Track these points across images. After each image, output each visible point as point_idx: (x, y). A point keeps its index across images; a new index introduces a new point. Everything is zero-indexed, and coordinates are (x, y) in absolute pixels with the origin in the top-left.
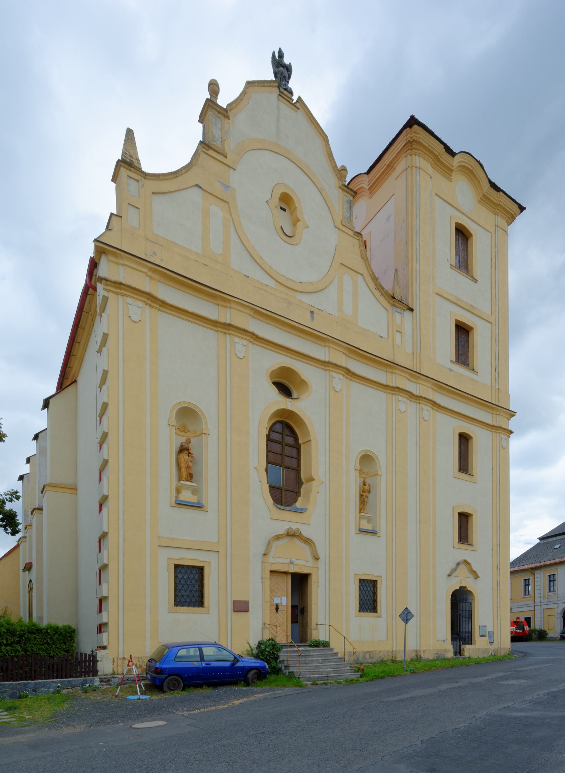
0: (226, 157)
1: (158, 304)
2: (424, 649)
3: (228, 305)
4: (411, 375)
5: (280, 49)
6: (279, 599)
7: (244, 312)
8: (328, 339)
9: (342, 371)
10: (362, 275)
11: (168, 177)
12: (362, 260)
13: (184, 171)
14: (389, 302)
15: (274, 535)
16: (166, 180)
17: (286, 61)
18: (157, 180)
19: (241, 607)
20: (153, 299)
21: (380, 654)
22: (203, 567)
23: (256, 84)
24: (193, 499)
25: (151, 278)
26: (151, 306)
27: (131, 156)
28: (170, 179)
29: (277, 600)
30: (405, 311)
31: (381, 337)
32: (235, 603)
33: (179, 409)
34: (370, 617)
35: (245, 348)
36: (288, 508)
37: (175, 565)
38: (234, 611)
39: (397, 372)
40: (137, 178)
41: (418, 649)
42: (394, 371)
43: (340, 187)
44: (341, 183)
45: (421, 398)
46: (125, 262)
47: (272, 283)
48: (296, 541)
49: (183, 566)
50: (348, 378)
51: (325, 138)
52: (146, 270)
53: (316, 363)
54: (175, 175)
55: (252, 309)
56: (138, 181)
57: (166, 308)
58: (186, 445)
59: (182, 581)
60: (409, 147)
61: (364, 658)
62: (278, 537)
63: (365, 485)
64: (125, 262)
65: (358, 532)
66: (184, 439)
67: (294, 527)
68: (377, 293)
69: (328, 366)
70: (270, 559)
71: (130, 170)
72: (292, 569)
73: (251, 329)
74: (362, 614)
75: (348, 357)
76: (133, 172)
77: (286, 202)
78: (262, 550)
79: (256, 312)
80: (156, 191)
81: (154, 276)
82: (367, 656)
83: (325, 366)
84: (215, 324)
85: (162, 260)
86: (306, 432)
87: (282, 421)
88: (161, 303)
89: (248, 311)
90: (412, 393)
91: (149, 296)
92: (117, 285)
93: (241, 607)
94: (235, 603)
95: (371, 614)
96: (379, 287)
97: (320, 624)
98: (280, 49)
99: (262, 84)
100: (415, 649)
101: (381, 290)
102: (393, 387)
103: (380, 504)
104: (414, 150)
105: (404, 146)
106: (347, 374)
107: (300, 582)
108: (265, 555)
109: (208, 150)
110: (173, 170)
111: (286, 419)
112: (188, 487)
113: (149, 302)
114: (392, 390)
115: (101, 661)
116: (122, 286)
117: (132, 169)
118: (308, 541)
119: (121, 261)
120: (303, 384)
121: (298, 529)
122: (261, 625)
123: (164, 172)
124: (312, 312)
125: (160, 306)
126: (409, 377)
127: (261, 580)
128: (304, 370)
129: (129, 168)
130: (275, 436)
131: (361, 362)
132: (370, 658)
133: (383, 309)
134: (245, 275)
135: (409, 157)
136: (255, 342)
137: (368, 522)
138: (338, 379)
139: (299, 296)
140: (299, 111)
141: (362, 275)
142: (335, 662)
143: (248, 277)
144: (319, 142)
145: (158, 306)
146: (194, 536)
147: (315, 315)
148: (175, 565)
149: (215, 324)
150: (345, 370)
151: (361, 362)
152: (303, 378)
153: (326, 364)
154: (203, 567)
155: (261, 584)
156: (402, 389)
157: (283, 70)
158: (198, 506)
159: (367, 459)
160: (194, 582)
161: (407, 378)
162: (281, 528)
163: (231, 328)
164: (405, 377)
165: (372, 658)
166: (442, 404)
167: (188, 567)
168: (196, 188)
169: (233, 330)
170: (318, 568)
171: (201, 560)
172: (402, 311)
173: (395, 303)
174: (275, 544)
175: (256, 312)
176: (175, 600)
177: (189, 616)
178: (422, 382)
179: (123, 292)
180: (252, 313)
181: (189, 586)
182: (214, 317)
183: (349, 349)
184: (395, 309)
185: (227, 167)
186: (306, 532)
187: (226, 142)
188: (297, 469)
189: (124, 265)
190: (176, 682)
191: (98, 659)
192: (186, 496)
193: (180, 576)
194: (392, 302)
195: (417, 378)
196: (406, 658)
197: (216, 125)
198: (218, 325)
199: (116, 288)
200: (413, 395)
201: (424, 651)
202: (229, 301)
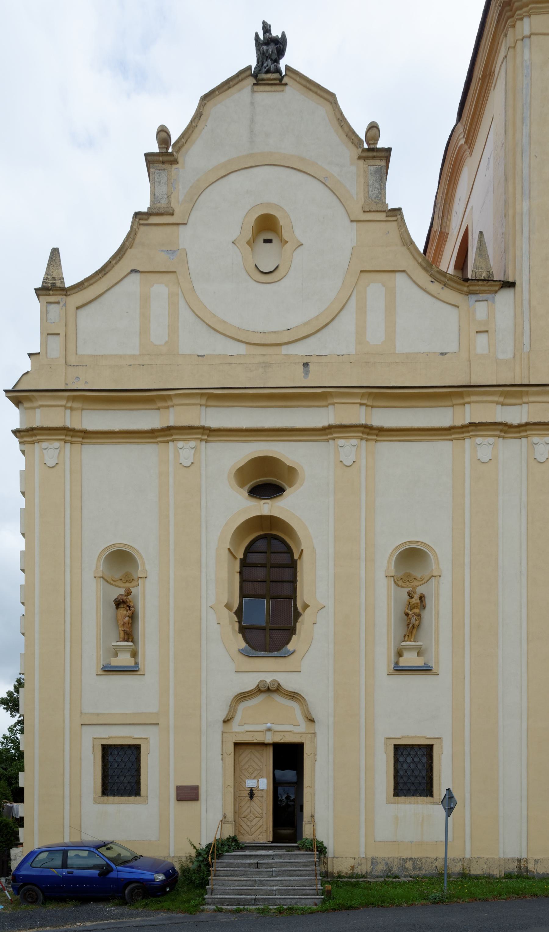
0: (172, 214)
1: (79, 437)
2: (537, 857)
3: (169, 403)
4: (506, 395)
5: (264, 23)
6: (255, 781)
7: (193, 404)
8: (329, 392)
9: (358, 432)
10: (404, 271)
11: (94, 280)
12: (404, 249)
13: (113, 262)
14: (461, 292)
15: (234, 695)
16: (92, 284)
17: (276, 33)
18: (81, 290)
19: (188, 794)
20: (71, 433)
21: (436, 864)
22: (140, 745)
23: (217, 92)
24: (419, 662)
25: (71, 409)
26: (72, 443)
27: (54, 279)
28: (97, 281)
29: (250, 783)
30: (496, 292)
31: (442, 354)
32: (179, 789)
33: (106, 557)
34: (418, 803)
35: (193, 450)
36: (276, 654)
37: (395, 745)
38: (178, 800)
39: (473, 398)
40: (57, 301)
41: (524, 856)
42: (467, 400)
43: (359, 158)
44: (360, 150)
45: (528, 427)
46: (40, 403)
47: (242, 349)
48: (278, 698)
49: (405, 746)
50: (372, 440)
51: (331, 99)
52: (63, 403)
53: (111, 438)
54: (103, 272)
55: (202, 395)
56: (58, 303)
57: (90, 438)
58: (124, 598)
59: (418, 765)
60: (509, 14)
61: (404, 869)
62: (243, 697)
63: (411, 597)
64: (40, 403)
65: (100, 672)
66: (122, 592)
67: (268, 679)
68: (436, 288)
69: (331, 433)
70: (235, 727)
71: (49, 295)
72: (269, 739)
73: (499, 419)
74: (106, 798)
75: (373, 407)
76: (53, 295)
77: (267, 228)
78: (223, 715)
79: (211, 397)
80: (80, 304)
81: (76, 405)
82: (409, 865)
83: (327, 435)
84: (151, 435)
85: (86, 382)
86: (298, 542)
87: (265, 534)
88: (83, 434)
89: (197, 401)
90: (505, 424)
91: (65, 432)
92: (31, 433)
93: (188, 794)
94: (179, 789)
95: (132, 798)
96: (438, 276)
97: (322, 816)
98: (264, 23)
99: (226, 87)
100: (517, 856)
101: (443, 278)
102: (463, 427)
103: (437, 621)
104: (518, 12)
105: (498, 21)
106: (368, 434)
107: (288, 757)
108: (226, 721)
109: (147, 220)
110: (98, 267)
111: (271, 530)
112: (410, 649)
113: (69, 438)
114: (463, 433)
115: (14, 860)
116: (35, 432)
117: (51, 292)
118: (294, 696)
119: (36, 404)
120: (291, 472)
121: (275, 681)
122: (220, 817)
123: (87, 276)
124: (306, 365)
125: (83, 438)
126: (501, 399)
127: (221, 756)
128: (285, 452)
129: (47, 292)
130: (254, 558)
131: (391, 406)
132: (414, 869)
133: (449, 307)
134: (198, 356)
135: (511, 31)
136: (379, 438)
137: (419, 654)
138: (349, 447)
139: (285, 350)
140: (287, 88)
141: (404, 271)
142: (302, 875)
143: (203, 356)
144: (322, 111)
145: (80, 440)
146: (123, 707)
147: (311, 366)
148: (395, 745)
149: (151, 435)
150: (362, 429)
151: (391, 406)
152: (288, 463)
153: (328, 431)
154: (140, 745)
155: (221, 762)
156: (481, 424)
157: (271, 47)
158: (426, 670)
159: (121, 559)
160: (420, 767)
161: (498, 403)
162: (250, 682)
163: (172, 431)
164: (493, 402)
165: (420, 869)
166: (515, 421)
167: (122, 747)
168: (134, 275)
169: (177, 434)
170: (315, 733)
171: (136, 736)
172: (489, 296)
173: (471, 288)
174: (243, 706)
175: (211, 397)
176: (395, 789)
177: (121, 809)
178: (532, 399)
179: (38, 438)
180: (203, 402)
181: (121, 770)
182: (447, 423)
183: (370, 393)
184: (473, 298)
185: (175, 227)
186: (289, 682)
187: (172, 196)
188: (292, 597)
189: (40, 406)
190: (31, 892)
191: (12, 857)
192: (410, 659)
193: (401, 759)
194: (465, 289)
195: (521, 395)
196: (335, 871)
197: (159, 182)
198: (157, 434)
199: (32, 436)
200: (511, 426)
201: (536, 862)
202: (170, 397)
